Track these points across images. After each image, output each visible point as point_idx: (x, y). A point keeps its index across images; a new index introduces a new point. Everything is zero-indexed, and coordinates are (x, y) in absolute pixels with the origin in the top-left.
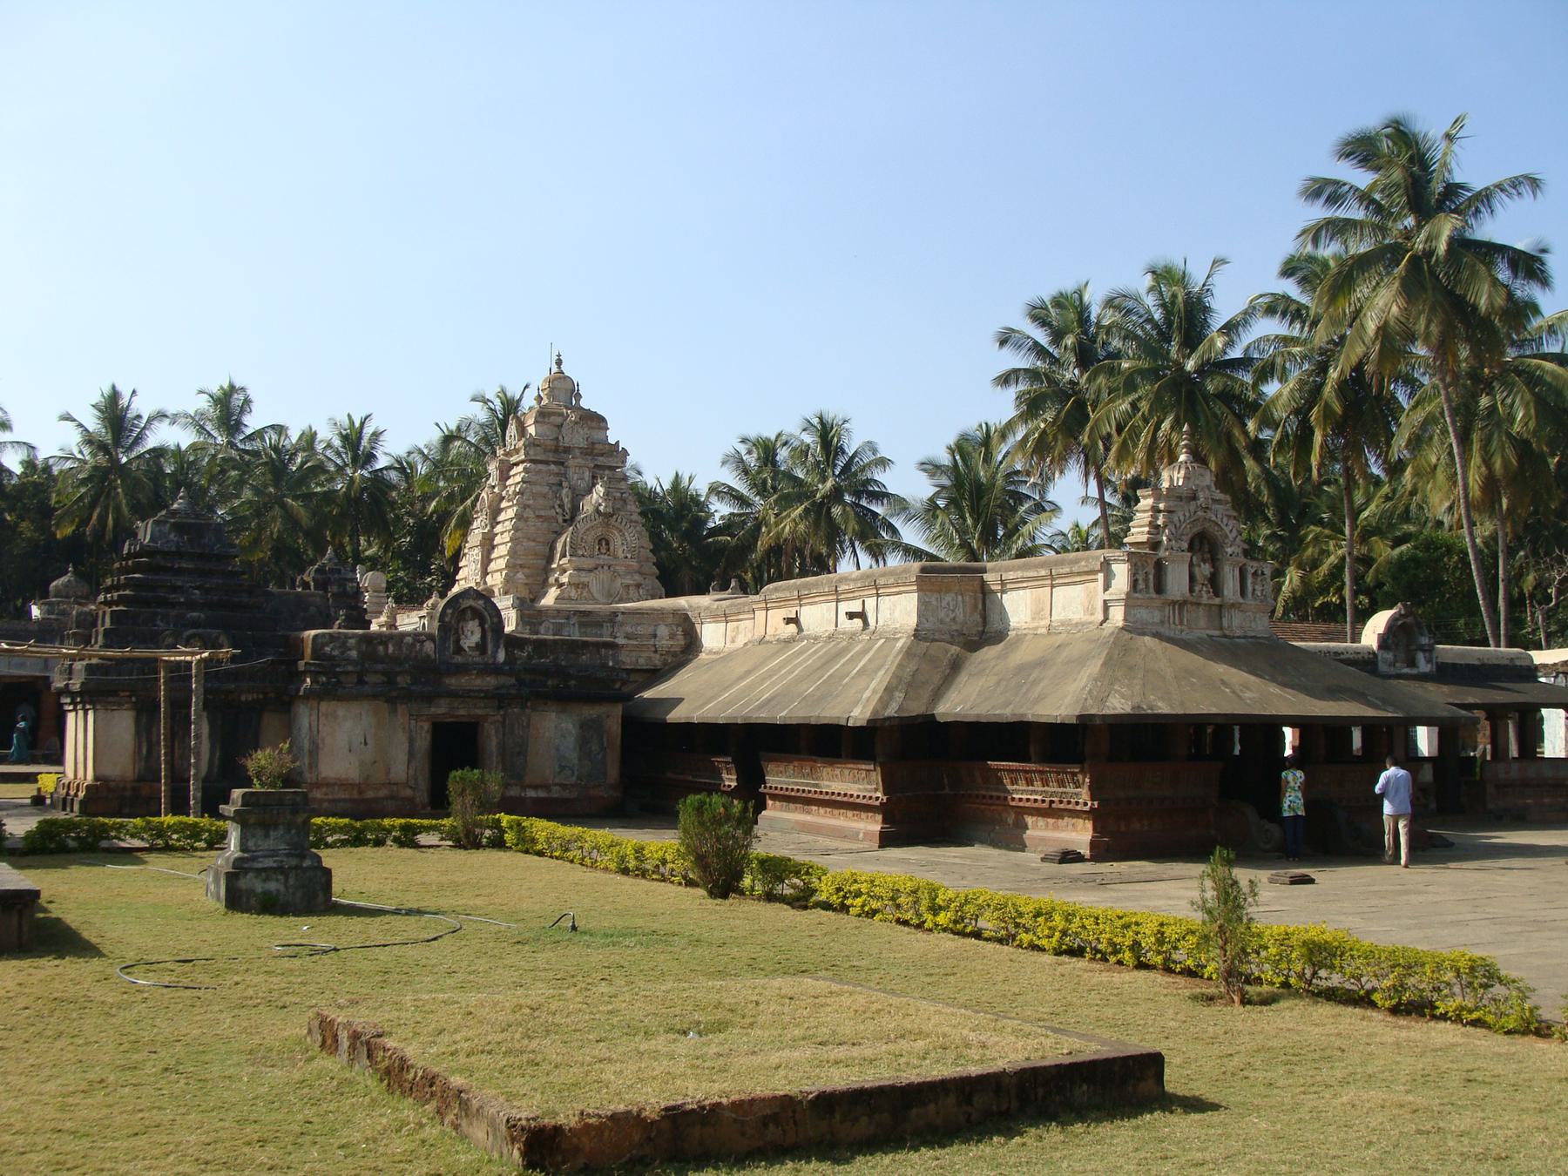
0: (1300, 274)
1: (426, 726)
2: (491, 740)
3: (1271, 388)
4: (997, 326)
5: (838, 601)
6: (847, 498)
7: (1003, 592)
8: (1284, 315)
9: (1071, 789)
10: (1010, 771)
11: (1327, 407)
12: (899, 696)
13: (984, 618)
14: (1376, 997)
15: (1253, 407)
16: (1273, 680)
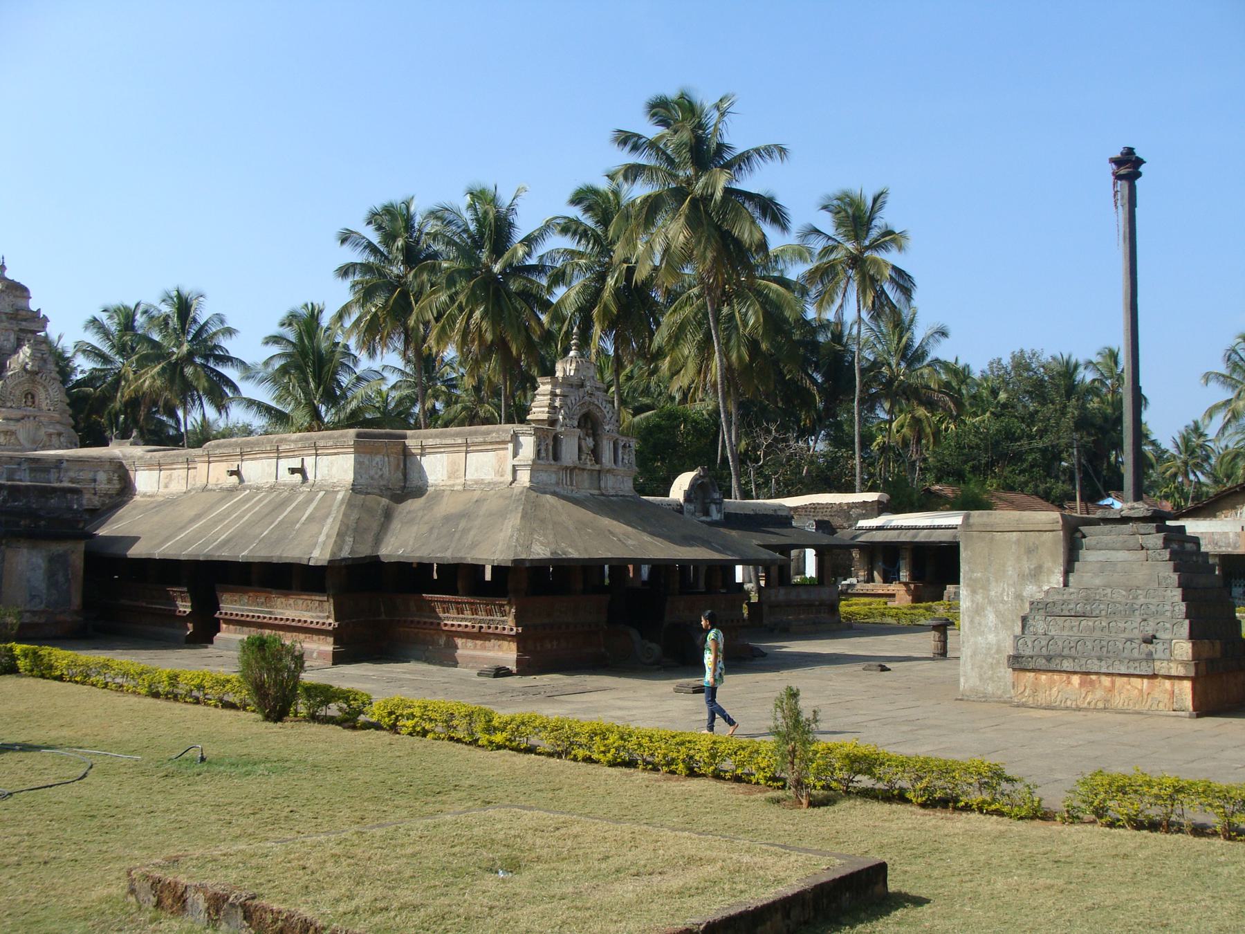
0: (586, 203)
3: (560, 292)
4: (338, 227)
5: (278, 458)
6: (198, 360)
7: (422, 455)
8: (575, 233)
9: (498, 617)
10: (443, 602)
11: (606, 306)
12: (349, 540)
13: (405, 475)
14: (910, 795)
15: (546, 306)
16: (644, 530)
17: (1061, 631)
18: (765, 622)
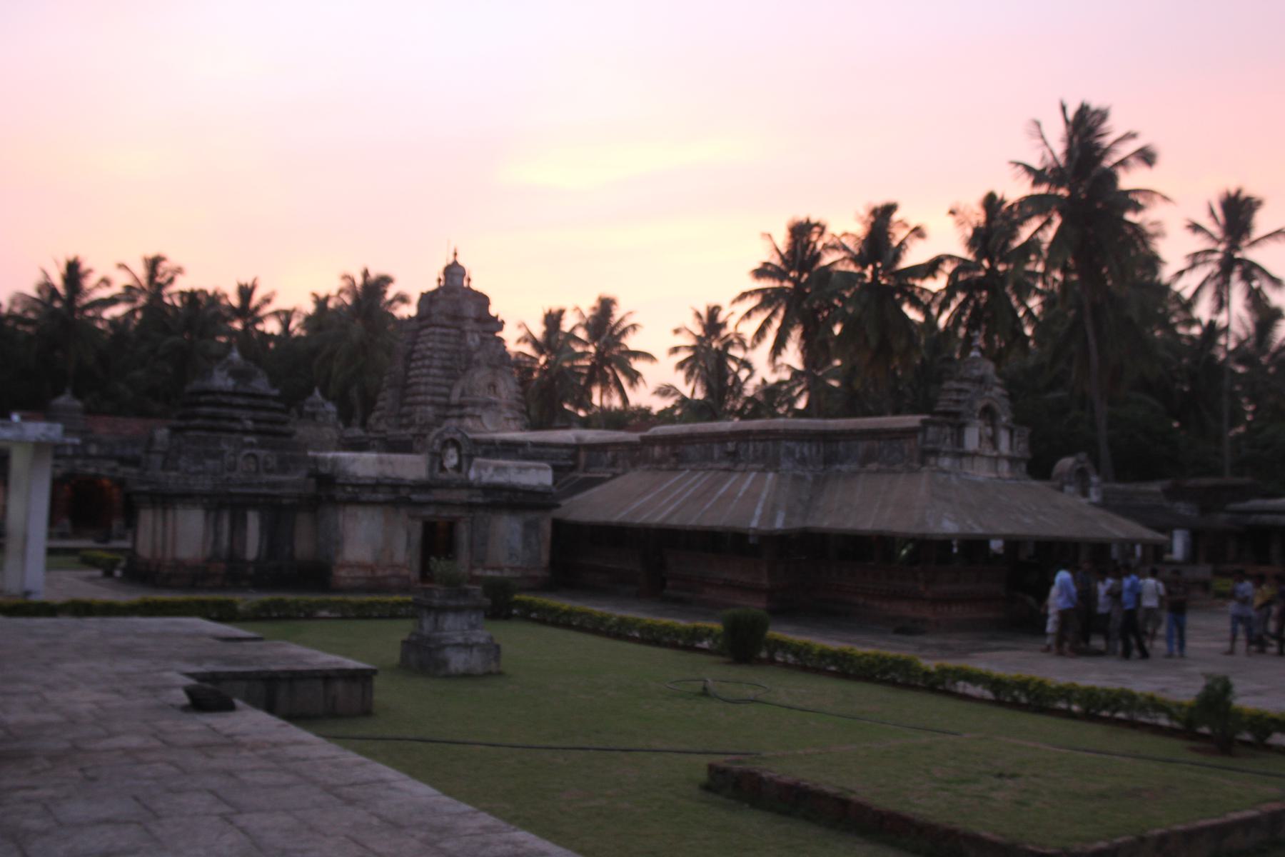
1: (419, 524)
2: (463, 535)
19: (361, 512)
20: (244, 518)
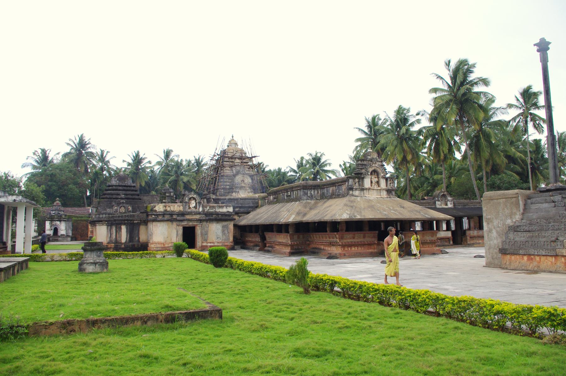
1: (181, 228)
17: (520, 237)
18: (468, 243)
19: (159, 224)
20: (121, 228)
